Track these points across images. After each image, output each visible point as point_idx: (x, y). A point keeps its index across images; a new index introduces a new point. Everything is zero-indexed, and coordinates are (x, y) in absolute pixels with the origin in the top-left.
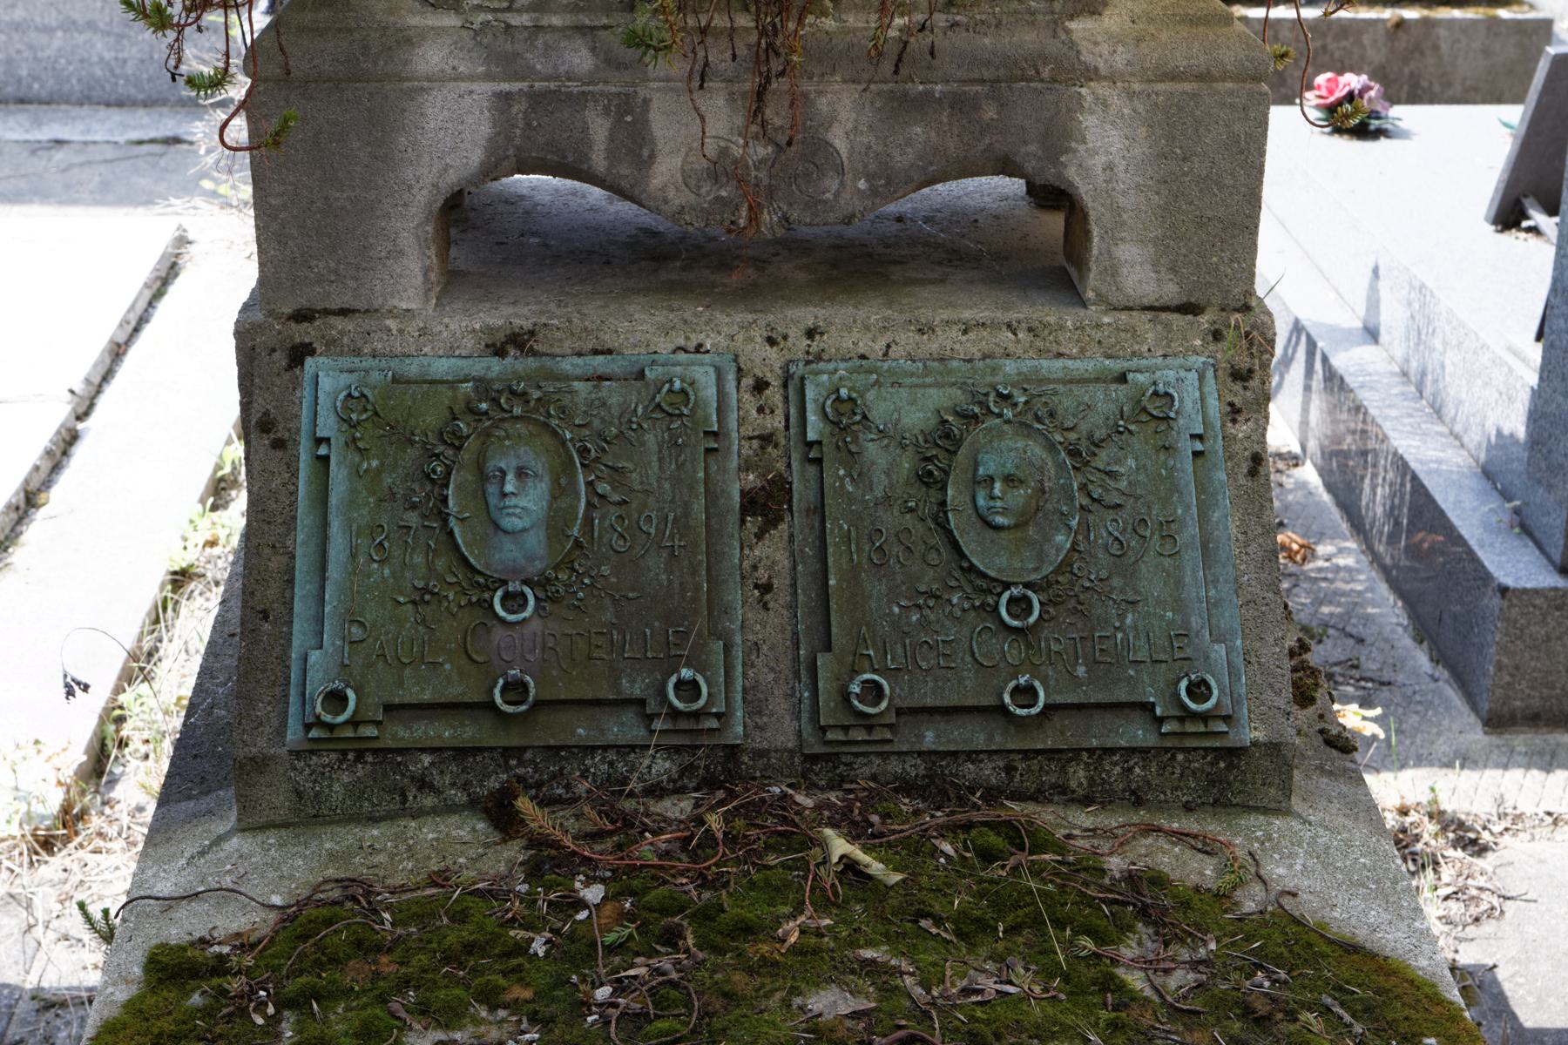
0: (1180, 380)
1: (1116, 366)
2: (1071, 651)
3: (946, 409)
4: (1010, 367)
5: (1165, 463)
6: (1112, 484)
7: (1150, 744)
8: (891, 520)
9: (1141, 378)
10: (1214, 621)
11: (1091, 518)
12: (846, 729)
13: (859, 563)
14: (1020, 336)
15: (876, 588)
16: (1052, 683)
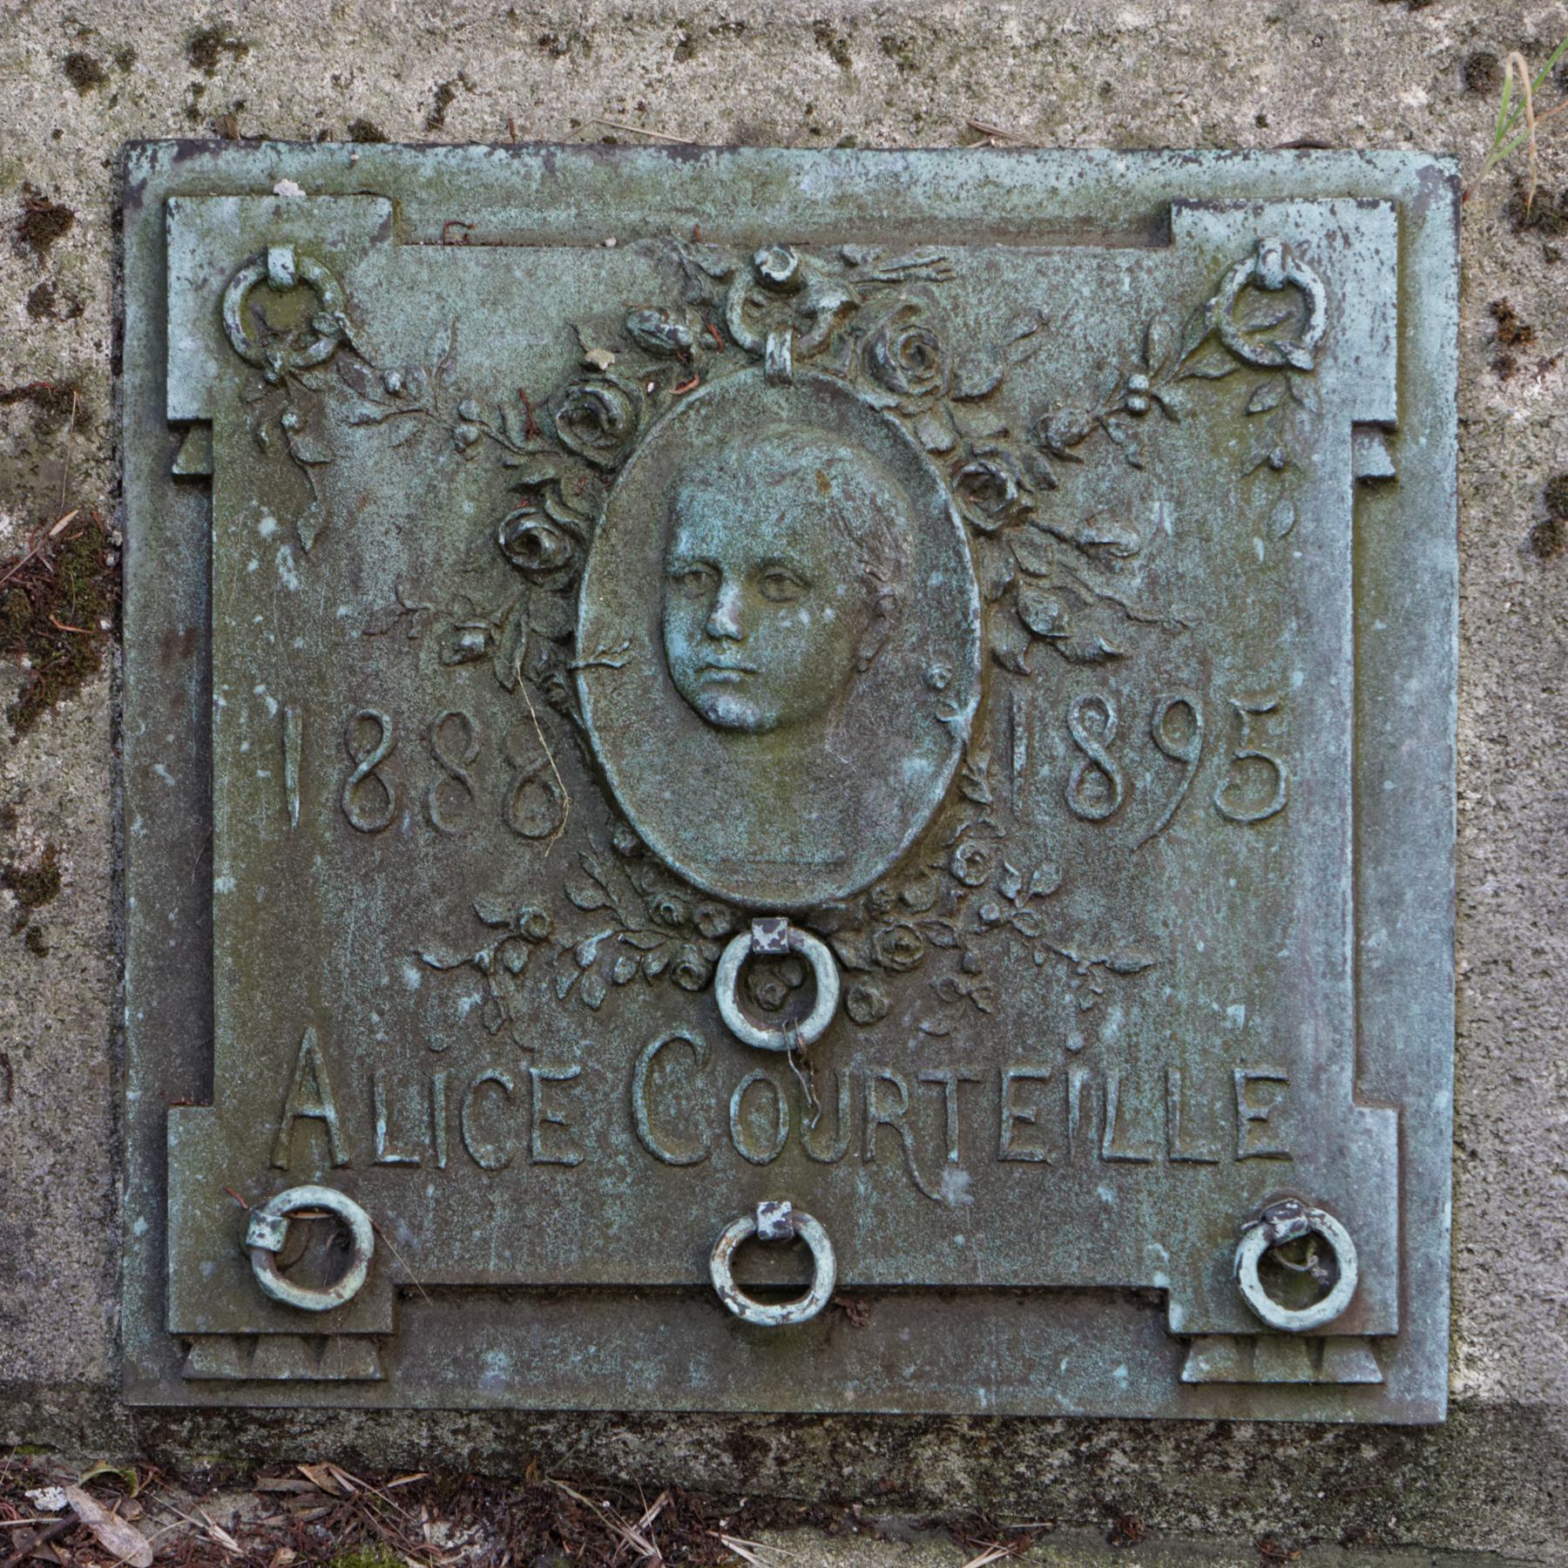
0: (1339, 237)
1: (1144, 177)
2: (928, 1120)
3: (599, 323)
4: (814, 176)
5: (1266, 517)
6: (1094, 580)
7: (1148, 1409)
8: (410, 685)
9: (1216, 228)
10: (1373, 1028)
11: (1022, 694)
12: (247, 1342)
13: (308, 822)
14: (859, 64)
15: (356, 905)
16: (866, 1219)
